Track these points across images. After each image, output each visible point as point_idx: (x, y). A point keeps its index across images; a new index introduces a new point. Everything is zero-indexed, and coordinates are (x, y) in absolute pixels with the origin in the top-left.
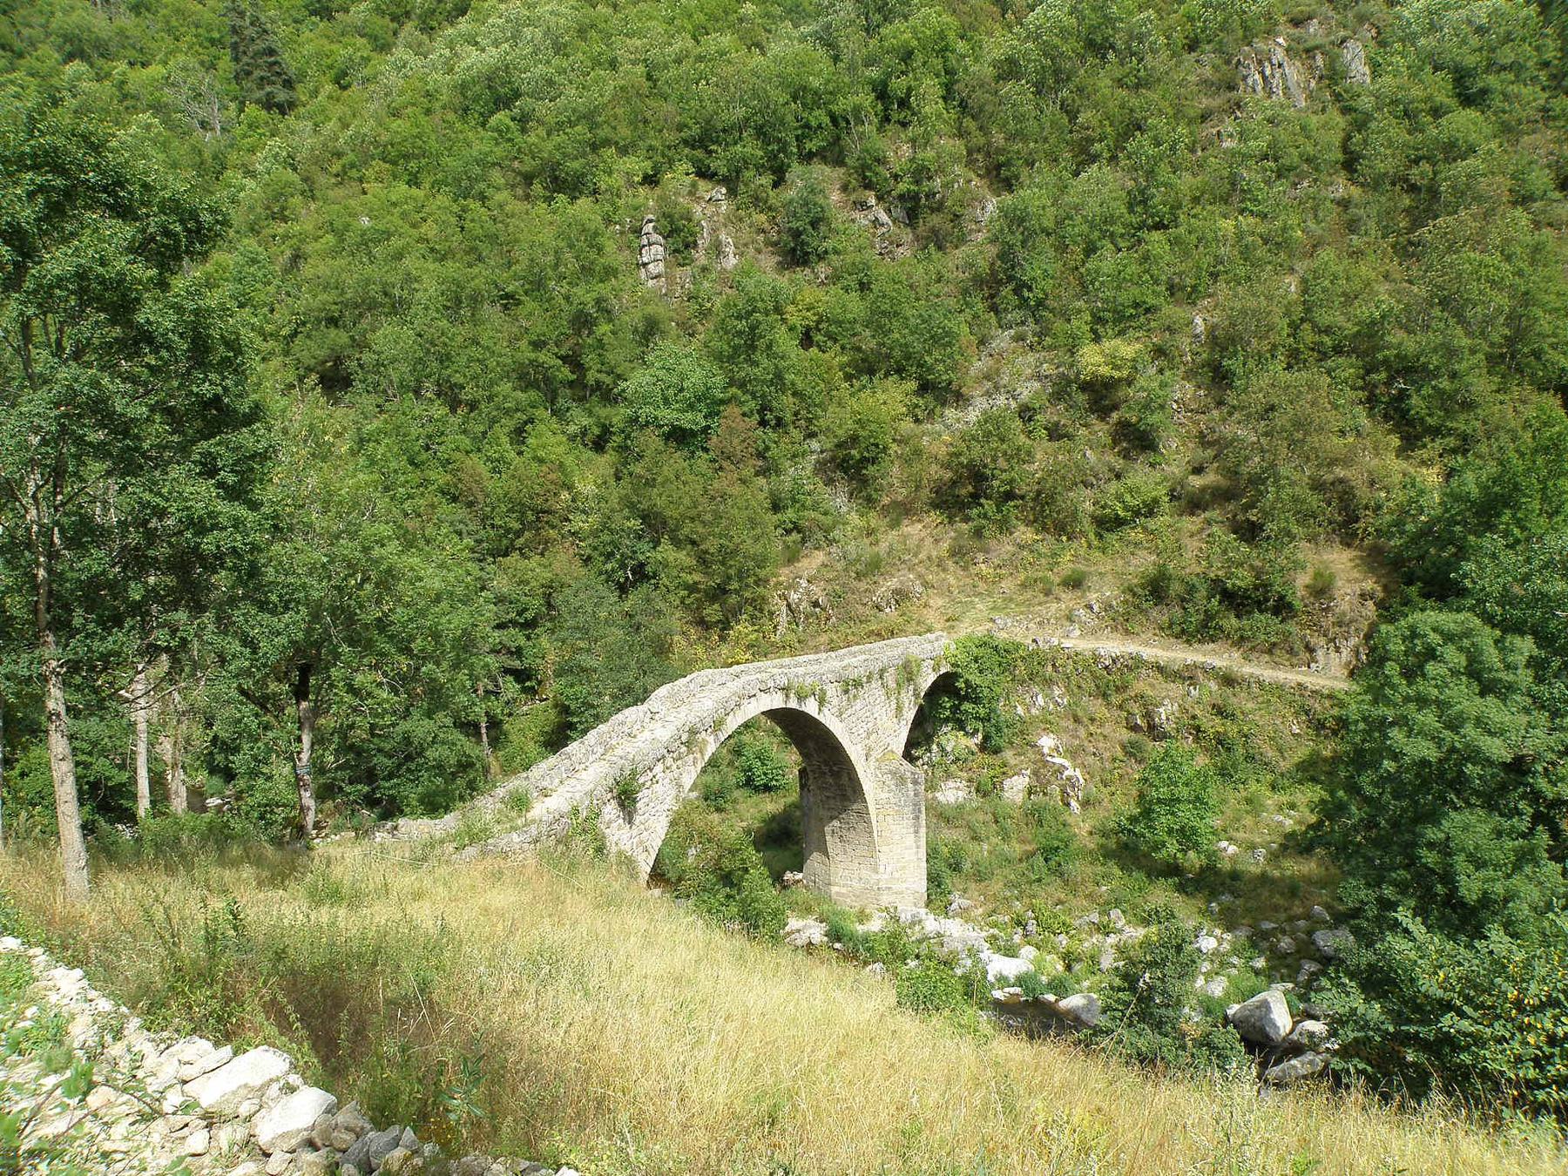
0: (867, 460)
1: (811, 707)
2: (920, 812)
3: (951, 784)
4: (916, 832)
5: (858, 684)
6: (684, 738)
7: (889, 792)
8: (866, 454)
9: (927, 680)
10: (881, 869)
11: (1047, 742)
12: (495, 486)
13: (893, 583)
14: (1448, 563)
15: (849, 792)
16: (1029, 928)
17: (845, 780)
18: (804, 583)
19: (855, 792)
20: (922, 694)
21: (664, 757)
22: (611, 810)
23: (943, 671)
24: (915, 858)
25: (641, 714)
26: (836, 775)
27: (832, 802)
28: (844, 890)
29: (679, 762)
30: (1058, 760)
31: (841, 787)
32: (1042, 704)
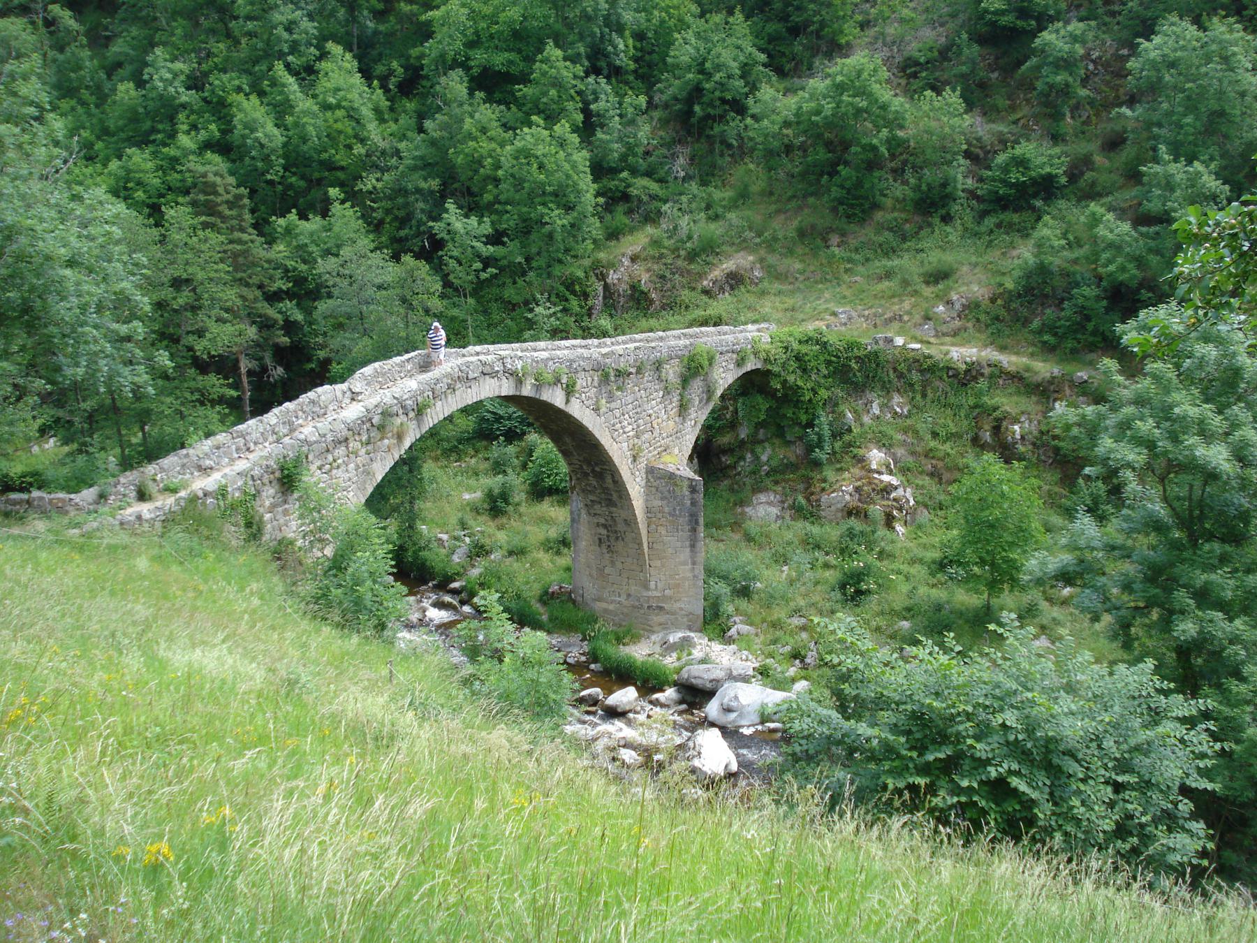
0: (713, 118)
1: (556, 397)
2: (697, 522)
3: (763, 498)
4: (693, 546)
5: (619, 374)
6: (376, 420)
7: (662, 499)
8: (710, 110)
9: (725, 377)
10: (652, 585)
11: (876, 456)
12: (270, 133)
13: (729, 265)
14: (8, 318)
15: (615, 497)
16: (808, 660)
17: (609, 480)
18: (626, 262)
19: (620, 497)
20: (719, 393)
21: (347, 439)
22: (269, 493)
23: (749, 366)
24: (690, 575)
25: (339, 394)
26: (600, 476)
27: (597, 507)
28: (611, 607)
29: (370, 447)
30: (886, 478)
31: (606, 490)
32: (877, 412)
